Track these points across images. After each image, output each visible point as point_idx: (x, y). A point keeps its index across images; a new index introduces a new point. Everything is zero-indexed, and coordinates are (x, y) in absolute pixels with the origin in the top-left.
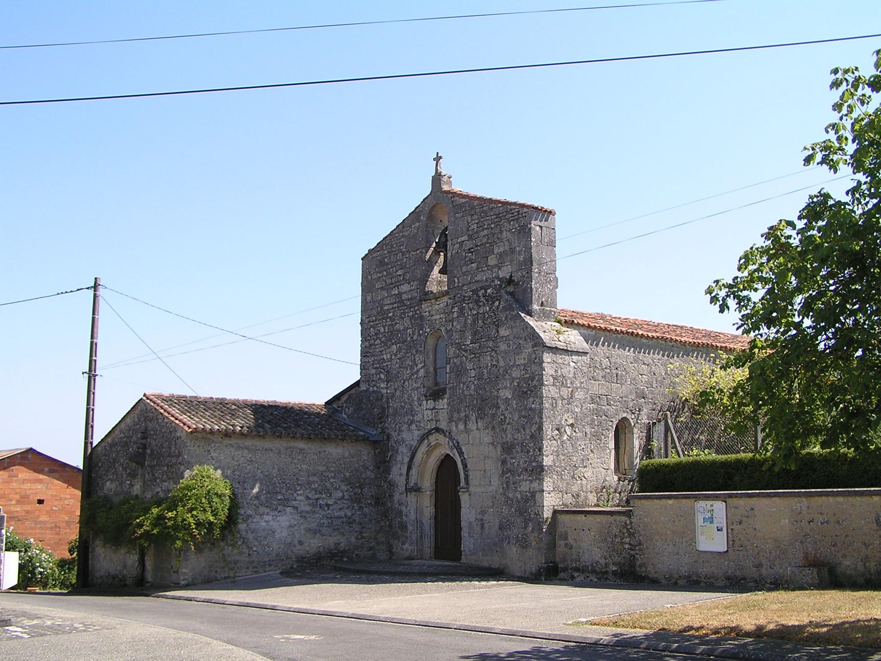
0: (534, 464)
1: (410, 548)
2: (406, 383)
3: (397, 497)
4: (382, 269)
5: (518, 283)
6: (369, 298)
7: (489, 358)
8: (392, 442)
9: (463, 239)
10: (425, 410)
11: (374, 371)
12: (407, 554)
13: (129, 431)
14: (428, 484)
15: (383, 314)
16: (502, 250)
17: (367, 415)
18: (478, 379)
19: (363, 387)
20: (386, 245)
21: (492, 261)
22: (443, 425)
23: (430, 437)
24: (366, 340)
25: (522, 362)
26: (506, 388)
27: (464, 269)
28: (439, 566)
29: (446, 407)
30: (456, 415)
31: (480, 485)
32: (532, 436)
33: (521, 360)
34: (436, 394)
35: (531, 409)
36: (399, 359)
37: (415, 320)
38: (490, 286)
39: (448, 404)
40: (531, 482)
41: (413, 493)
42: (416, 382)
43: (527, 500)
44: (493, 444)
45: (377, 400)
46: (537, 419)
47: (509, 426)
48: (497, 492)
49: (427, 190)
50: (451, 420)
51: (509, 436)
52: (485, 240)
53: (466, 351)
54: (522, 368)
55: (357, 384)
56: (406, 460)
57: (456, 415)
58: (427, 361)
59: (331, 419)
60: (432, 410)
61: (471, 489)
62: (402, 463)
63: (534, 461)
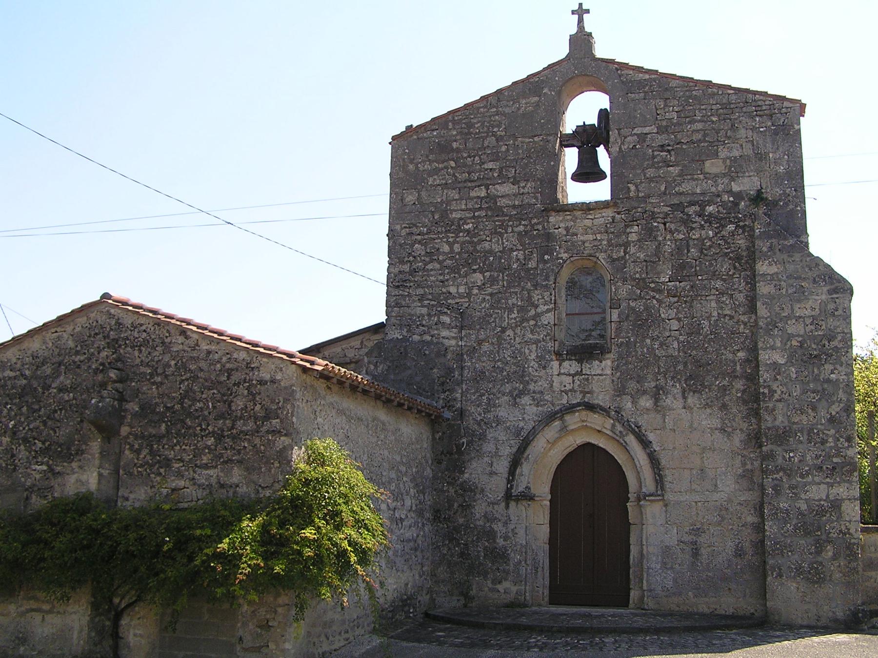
0: (835, 460)
1: (514, 589)
2: (509, 332)
3: (480, 509)
4: (444, 156)
5: (775, 203)
6: (410, 198)
7: (714, 304)
8: (469, 422)
9: (646, 130)
10: (561, 376)
11: (424, 311)
12: (510, 598)
13: (382, 611)
14: (543, 489)
15: (445, 223)
16: (736, 153)
17: (418, 379)
18: (689, 334)
19: (395, 334)
20: (454, 122)
21: (713, 166)
22: (601, 398)
23: (567, 418)
24: (402, 262)
25: (808, 312)
26: (773, 348)
27: (650, 172)
28: (613, 616)
29: (609, 372)
30: (632, 385)
31: (692, 491)
32: (832, 420)
33: (805, 310)
34: (586, 352)
35: (828, 381)
36: (491, 295)
37: (533, 238)
38: (709, 203)
39: (615, 369)
40: (831, 485)
41: (524, 503)
42: (532, 332)
43: (822, 512)
44: (723, 430)
45: (438, 354)
46: (841, 395)
47: (780, 405)
48: (730, 501)
49: (561, 51)
50: (620, 391)
51: (780, 418)
52: (697, 137)
53: (660, 291)
54: (808, 321)
55: (378, 328)
56: (507, 451)
57: (632, 385)
58: (558, 301)
59: (745, 267)
60: (573, 376)
61: (669, 496)
62: (496, 455)
63: (837, 455)
